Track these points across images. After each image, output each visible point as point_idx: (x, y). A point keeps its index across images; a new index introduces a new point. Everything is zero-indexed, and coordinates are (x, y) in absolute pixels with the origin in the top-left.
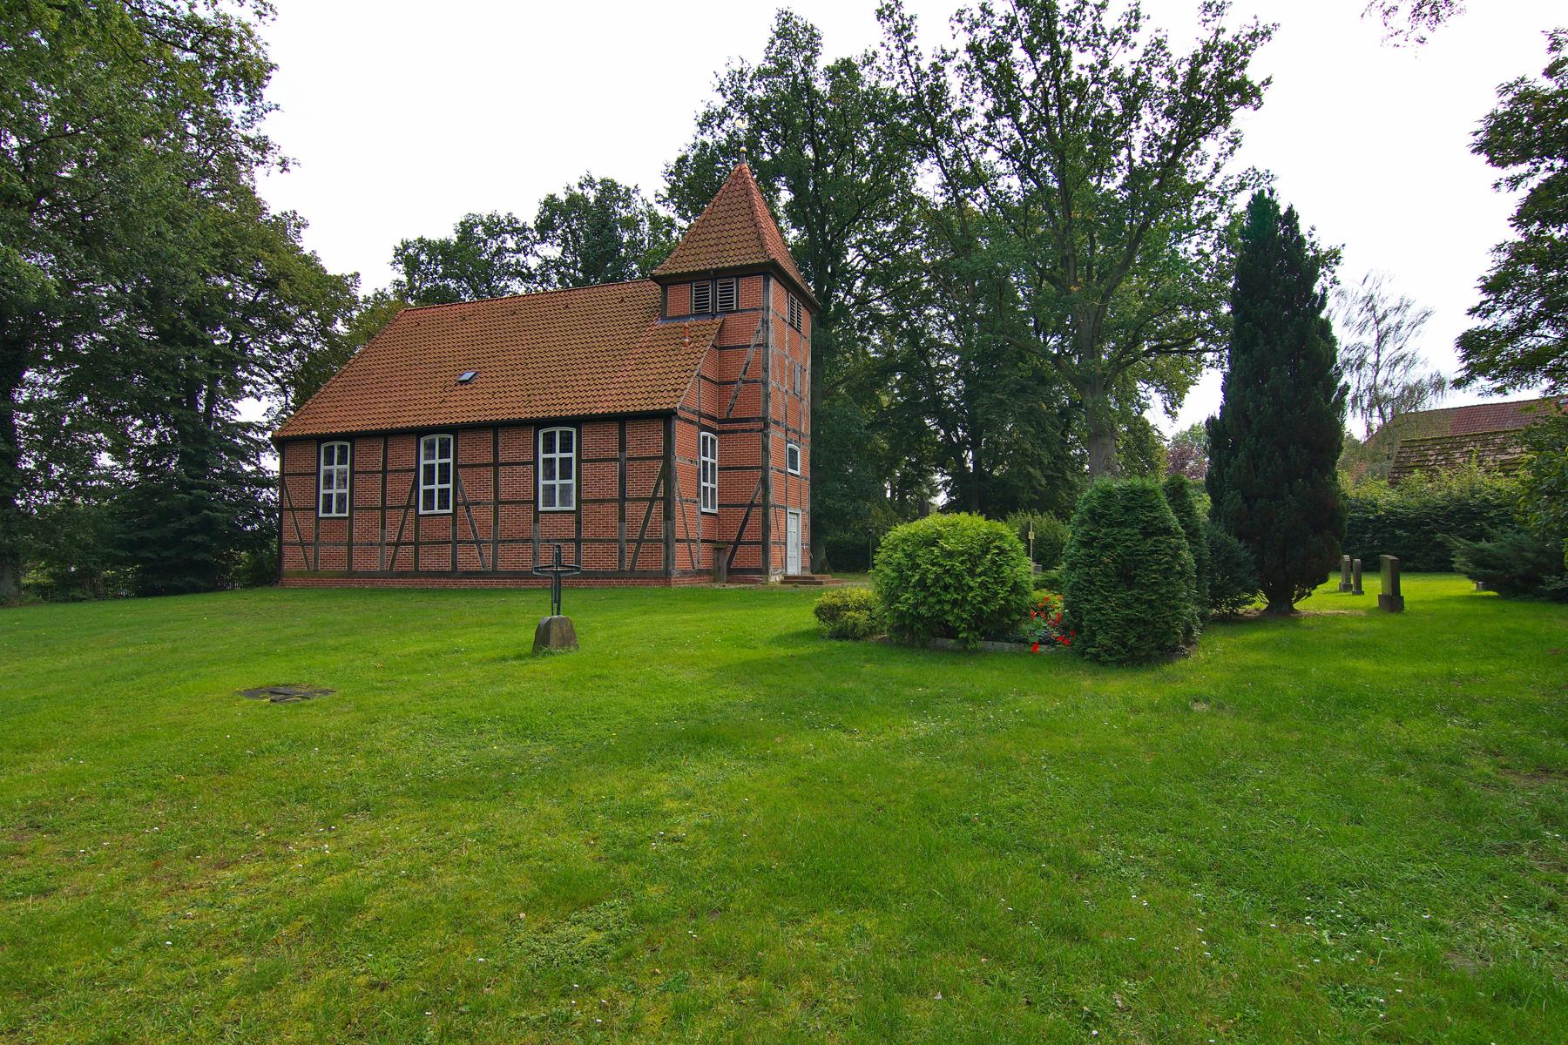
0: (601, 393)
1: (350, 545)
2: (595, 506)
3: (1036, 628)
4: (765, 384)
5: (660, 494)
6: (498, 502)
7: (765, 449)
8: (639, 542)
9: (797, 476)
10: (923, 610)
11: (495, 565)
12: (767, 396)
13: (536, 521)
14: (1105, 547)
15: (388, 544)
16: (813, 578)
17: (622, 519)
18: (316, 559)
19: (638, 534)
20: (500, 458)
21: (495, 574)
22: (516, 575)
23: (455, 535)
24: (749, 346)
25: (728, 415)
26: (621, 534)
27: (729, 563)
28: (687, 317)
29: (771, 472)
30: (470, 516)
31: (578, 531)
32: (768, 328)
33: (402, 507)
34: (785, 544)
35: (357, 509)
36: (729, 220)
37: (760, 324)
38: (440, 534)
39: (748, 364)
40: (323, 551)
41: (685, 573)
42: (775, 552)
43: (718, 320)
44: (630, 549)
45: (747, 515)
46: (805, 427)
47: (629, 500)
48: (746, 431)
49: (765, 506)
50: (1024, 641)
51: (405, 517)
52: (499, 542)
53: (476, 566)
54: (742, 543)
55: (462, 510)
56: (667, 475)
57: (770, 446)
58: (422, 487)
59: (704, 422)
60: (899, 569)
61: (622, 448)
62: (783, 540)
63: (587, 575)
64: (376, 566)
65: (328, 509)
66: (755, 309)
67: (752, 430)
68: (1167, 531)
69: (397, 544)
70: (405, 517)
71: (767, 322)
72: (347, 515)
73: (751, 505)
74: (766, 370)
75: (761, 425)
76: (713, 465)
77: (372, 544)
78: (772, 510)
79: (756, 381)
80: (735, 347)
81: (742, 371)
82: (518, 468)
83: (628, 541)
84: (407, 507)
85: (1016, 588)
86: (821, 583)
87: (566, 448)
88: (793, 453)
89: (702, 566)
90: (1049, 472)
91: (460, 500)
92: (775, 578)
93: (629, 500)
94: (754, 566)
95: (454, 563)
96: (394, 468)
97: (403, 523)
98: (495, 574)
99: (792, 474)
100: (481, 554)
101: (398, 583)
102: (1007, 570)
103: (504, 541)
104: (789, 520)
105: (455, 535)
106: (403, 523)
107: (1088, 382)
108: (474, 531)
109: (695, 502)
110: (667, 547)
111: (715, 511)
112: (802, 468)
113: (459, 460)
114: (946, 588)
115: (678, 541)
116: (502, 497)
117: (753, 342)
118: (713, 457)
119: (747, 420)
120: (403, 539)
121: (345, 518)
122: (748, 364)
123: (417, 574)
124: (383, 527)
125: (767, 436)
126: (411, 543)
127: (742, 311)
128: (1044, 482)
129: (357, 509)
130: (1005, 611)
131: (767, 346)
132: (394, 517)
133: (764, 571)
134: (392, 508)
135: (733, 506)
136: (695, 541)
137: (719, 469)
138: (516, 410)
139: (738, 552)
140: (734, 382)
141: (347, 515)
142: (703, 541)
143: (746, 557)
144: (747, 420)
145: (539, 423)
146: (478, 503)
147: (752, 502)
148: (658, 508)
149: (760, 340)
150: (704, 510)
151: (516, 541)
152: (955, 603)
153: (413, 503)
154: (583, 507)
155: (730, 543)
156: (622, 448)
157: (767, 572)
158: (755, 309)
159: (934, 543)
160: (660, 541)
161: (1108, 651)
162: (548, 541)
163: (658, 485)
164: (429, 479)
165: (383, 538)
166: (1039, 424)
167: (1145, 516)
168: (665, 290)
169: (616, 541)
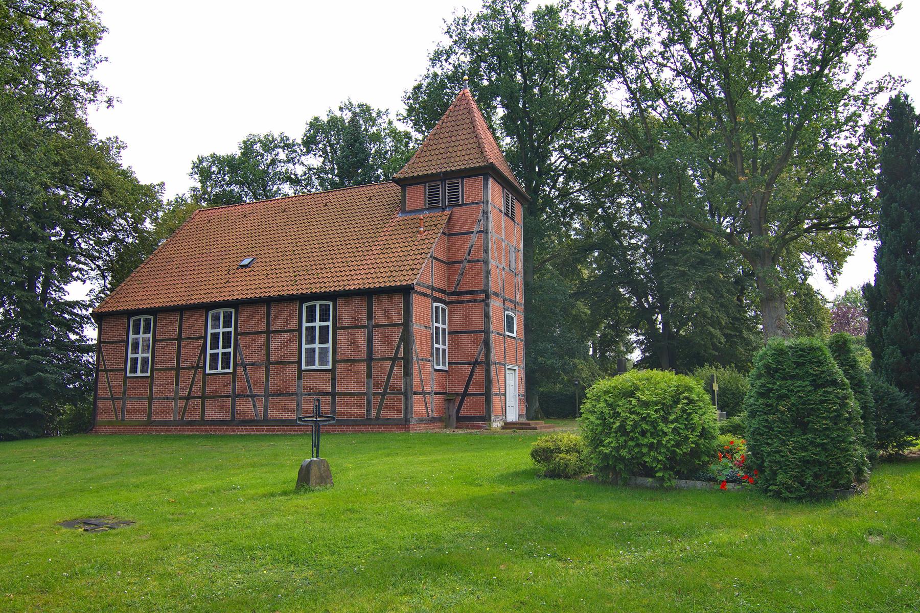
1: (150, 399)
2: (347, 365)
3: (722, 468)
4: (486, 263)
5: (401, 355)
6: (269, 363)
7: (487, 316)
9: (514, 338)
10: (624, 453)
11: (265, 415)
12: (488, 272)
13: (300, 378)
14: (781, 397)
15: (180, 398)
16: (529, 424)
17: (369, 376)
18: (123, 411)
21: (265, 422)
23: (234, 390)
26: (368, 388)
28: (422, 210)
29: (491, 335)
30: (246, 375)
31: (334, 386)
32: (487, 218)
33: (192, 368)
34: (505, 395)
37: (481, 214)
38: (222, 389)
39: (471, 247)
41: (421, 420)
42: (496, 403)
43: (447, 212)
45: (472, 371)
49: (488, 363)
50: (713, 480)
52: (269, 396)
53: (251, 416)
55: (240, 370)
57: (491, 314)
58: (209, 352)
59: (436, 294)
60: (602, 417)
61: (370, 317)
62: (502, 391)
64: (170, 416)
66: (477, 203)
67: (475, 301)
68: (834, 383)
69: (188, 398)
71: (487, 213)
73: (476, 363)
74: (486, 251)
75: (483, 296)
77: (167, 398)
78: (493, 367)
79: (478, 261)
82: (286, 335)
83: (374, 394)
86: (535, 429)
89: (435, 415)
90: (728, 332)
91: (239, 361)
92: (496, 424)
97: (193, 381)
98: (265, 422)
99: (509, 336)
100: (254, 406)
102: (696, 418)
105: (234, 390)
106: (193, 381)
108: (249, 387)
109: (429, 361)
110: (406, 399)
111: (446, 368)
113: (239, 329)
114: (643, 433)
115: (415, 393)
116: (272, 359)
117: (476, 229)
119: (471, 293)
120: (192, 394)
122: (471, 247)
123: (203, 422)
124: (177, 384)
125: (487, 305)
126: (199, 397)
127: (466, 205)
128: (723, 340)
130: (695, 453)
131: (487, 233)
132: (186, 375)
136: (429, 394)
139: (465, 402)
142: (436, 393)
143: (472, 407)
144: (471, 293)
146: (253, 364)
147: (476, 360)
148: (399, 366)
149: (481, 227)
150: (436, 367)
152: (651, 446)
153: (201, 364)
154: (338, 366)
155: (458, 395)
156: (370, 317)
157: (490, 419)
158: (477, 203)
159: (632, 394)
160: (400, 393)
161: (789, 488)
162: (309, 395)
163: (398, 347)
165: (176, 393)
168: (404, 190)
169: (364, 394)
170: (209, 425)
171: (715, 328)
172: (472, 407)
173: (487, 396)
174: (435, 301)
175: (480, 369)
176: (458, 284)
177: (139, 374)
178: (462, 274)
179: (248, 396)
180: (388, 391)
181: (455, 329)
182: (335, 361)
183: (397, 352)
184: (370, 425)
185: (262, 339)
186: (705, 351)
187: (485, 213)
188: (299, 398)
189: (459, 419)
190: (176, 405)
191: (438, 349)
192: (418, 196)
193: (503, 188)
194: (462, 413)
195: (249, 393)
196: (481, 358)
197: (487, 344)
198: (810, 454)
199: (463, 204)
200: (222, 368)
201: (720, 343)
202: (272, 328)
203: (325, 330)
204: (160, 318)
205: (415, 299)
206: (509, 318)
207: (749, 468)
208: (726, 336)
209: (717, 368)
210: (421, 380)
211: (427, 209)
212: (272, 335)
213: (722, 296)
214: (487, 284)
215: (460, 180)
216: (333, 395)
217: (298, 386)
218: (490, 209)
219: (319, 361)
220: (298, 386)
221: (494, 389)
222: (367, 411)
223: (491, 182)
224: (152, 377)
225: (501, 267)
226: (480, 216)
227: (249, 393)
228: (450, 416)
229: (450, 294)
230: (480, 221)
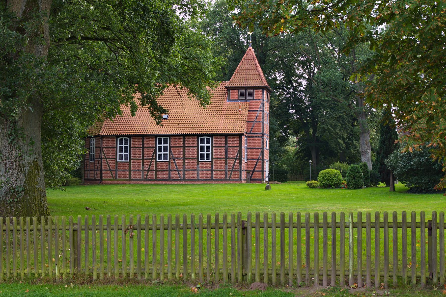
0: (217, 126)
1: (130, 171)
3: (342, 186)
5: (238, 157)
6: (184, 158)
7: (263, 143)
8: (232, 171)
10: (327, 183)
11: (184, 177)
13: (198, 164)
14: (352, 174)
15: (145, 171)
17: (226, 164)
18: (116, 175)
19: (231, 169)
20: (185, 145)
21: (184, 180)
22: (191, 180)
23: (170, 168)
24: (258, 111)
26: (226, 168)
27: (251, 177)
28: (237, 100)
30: (175, 162)
31: (212, 167)
33: (150, 159)
35: (132, 159)
36: (249, 68)
37: (261, 104)
38: (164, 167)
39: (257, 116)
40: (119, 172)
44: (229, 173)
45: (257, 162)
47: (229, 159)
48: (257, 137)
50: (341, 187)
52: (185, 170)
53: (178, 177)
54: (255, 171)
55: (172, 161)
58: (158, 153)
60: (323, 177)
61: (226, 143)
63: (215, 180)
64: (140, 177)
66: (260, 100)
67: (258, 137)
68: (360, 172)
69: (148, 171)
71: (263, 104)
72: (129, 161)
73: (258, 159)
74: (263, 118)
75: (261, 135)
77: (138, 170)
79: (260, 122)
80: (253, 111)
82: (192, 148)
83: (228, 170)
84: (152, 159)
85: (340, 180)
87: (126, 143)
90: (346, 141)
91: (171, 157)
92: (264, 182)
93: (229, 159)
94: (259, 178)
96: (147, 147)
98: (198, 180)
101: (149, 183)
102: (339, 177)
103: (187, 170)
105: (170, 168)
107: (360, 114)
108: (176, 167)
113: (171, 145)
114: (330, 180)
116: (186, 157)
117: (259, 110)
119: (257, 134)
120: (150, 169)
122: (257, 116)
123: (156, 180)
124: (143, 165)
125: (263, 139)
127: (255, 100)
128: (344, 145)
129: (132, 159)
130: (338, 183)
131: (263, 111)
132: (147, 163)
134: (260, 171)
135: (252, 160)
138: (185, 131)
140: (253, 122)
141: (129, 161)
143: (256, 175)
144: (257, 134)
145: (199, 135)
146: (178, 158)
147: (258, 159)
148: (238, 161)
149: (261, 109)
151: (191, 170)
152: (331, 182)
153: (154, 157)
155: (251, 171)
156: (226, 143)
158: (260, 100)
159: (328, 173)
160: (238, 170)
161: (352, 188)
162: (202, 170)
163: (237, 155)
165: (143, 168)
166: (343, 122)
167: (357, 170)
169: (225, 170)
171: (341, 140)
175: (260, 162)
179: (176, 170)
182: (212, 159)
183: (237, 156)
185: (182, 149)
186: (336, 150)
187: (263, 104)
189: (251, 180)
190: (143, 173)
192: (235, 94)
194: (252, 178)
196: (260, 158)
198: (355, 183)
199: (254, 100)
201: (343, 147)
202: (186, 145)
203: (208, 148)
205: (243, 137)
207: (346, 186)
208: (345, 143)
209: (341, 163)
211: (239, 100)
212: (186, 148)
213: (345, 124)
214: (263, 131)
215: (253, 90)
216: (212, 170)
217: (198, 167)
219: (206, 158)
223: (265, 92)
226: (261, 105)
229: (248, 133)
230: (261, 107)
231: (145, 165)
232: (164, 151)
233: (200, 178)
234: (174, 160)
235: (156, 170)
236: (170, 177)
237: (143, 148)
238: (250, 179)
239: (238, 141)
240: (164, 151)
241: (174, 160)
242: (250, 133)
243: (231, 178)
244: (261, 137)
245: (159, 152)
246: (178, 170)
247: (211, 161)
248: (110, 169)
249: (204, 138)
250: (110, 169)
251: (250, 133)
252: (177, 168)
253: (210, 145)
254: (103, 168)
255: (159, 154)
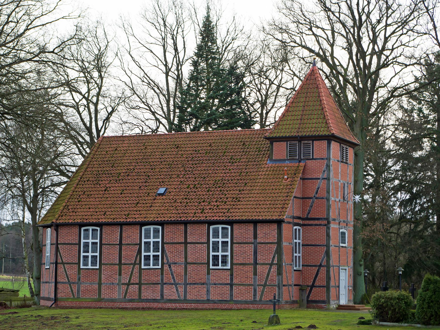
2: (241, 267)
4: (328, 200)
5: (275, 262)
6: (186, 263)
7: (328, 235)
9: (345, 247)
11: (185, 296)
12: (329, 207)
13: (208, 273)
15: (123, 284)
16: (354, 307)
17: (255, 274)
18: (78, 291)
20: (188, 240)
23: (162, 280)
24: (319, 179)
25: (307, 215)
26: (255, 282)
28: (285, 160)
29: (331, 248)
30: (171, 270)
31: (232, 279)
32: (329, 169)
33: (131, 264)
34: (339, 287)
35: (104, 264)
37: (325, 167)
39: (318, 188)
41: (287, 302)
42: (333, 291)
43: (302, 164)
46: (351, 218)
47: (260, 264)
49: (328, 266)
51: (133, 269)
52: (187, 284)
54: (315, 287)
55: (166, 267)
56: (279, 251)
57: (331, 234)
58: (143, 254)
59: (296, 221)
61: (255, 237)
62: (337, 284)
65: (86, 264)
66: (322, 159)
67: (320, 225)
69: (128, 284)
70: (133, 269)
71: (329, 167)
72: (98, 267)
73: (320, 266)
74: (328, 192)
76: (299, 243)
78: (331, 269)
79: (323, 198)
81: (315, 191)
82: (198, 246)
83: (258, 285)
84: (135, 264)
86: (359, 310)
87: (225, 235)
88: (343, 234)
89: (294, 299)
91: (165, 261)
92: (333, 305)
93: (260, 264)
95: (162, 295)
96: (126, 243)
97: (132, 273)
99: (342, 247)
100: (177, 290)
103: (190, 284)
104: (341, 273)
105: (162, 280)
106: (132, 273)
108: (173, 278)
109: (291, 265)
110: (279, 289)
111: (301, 268)
112: (348, 243)
113: (165, 241)
115: (284, 286)
118: (299, 253)
119: (318, 219)
120: (132, 281)
121: (97, 269)
122: (318, 188)
124: (120, 274)
125: (328, 228)
126: (137, 284)
127: (315, 159)
129: (104, 264)
133: (327, 302)
136: (291, 285)
137: (302, 245)
139: (313, 291)
141: (98, 267)
142: (295, 285)
143: (317, 294)
144: (318, 219)
146: (175, 263)
148: (274, 269)
149: (325, 176)
150: (295, 268)
151: (197, 284)
153: (138, 262)
154: (234, 267)
155: (308, 286)
156: (255, 237)
157: (329, 303)
158: (322, 159)
160: (275, 286)
162: (215, 284)
163: (274, 257)
164: (148, 249)
165: (120, 280)
168: (272, 144)
170: (144, 302)
172: (317, 294)
173: (328, 287)
174: (295, 225)
176: (309, 213)
177: (90, 267)
178: (312, 206)
180: (268, 284)
181: (307, 243)
183: (273, 260)
184: (255, 304)
185: (182, 247)
187: (328, 166)
188: (208, 286)
190: (120, 288)
191: (296, 257)
193: (340, 144)
194: (310, 298)
195: (173, 282)
197: (328, 254)
199: (313, 159)
200: (153, 265)
202: (188, 241)
204: (105, 229)
205: (284, 225)
206: (343, 234)
210: (287, 277)
211: (288, 160)
212: (188, 245)
214: (328, 214)
215: (311, 142)
216: (231, 285)
217: (208, 279)
218: (331, 163)
220: (208, 279)
221: (332, 283)
222: (254, 295)
224: (100, 269)
225: (338, 200)
226: (324, 167)
227: (173, 282)
228: (303, 300)
230: (324, 171)
231: (123, 275)
232: (93, 252)
233: (211, 298)
234: (170, 267)
235: (140, 284)
236: (162, 295)
237: (121, 244)
238: (305, 301)
239: (275, 233)
240: (93, 252)
241: (170, 267)
242: (307, 219)
243: (263, 299)
244: (325, 225)
245: (213, 252)
246: (176, 284)
247: (229, 267)
248: (69, 281)
249: (150, 228)
250: (69, 281)
251: (307, 219)
252: (174, 280)
253: (229, 240)
254: (59, 279)
255: (213, 256)
